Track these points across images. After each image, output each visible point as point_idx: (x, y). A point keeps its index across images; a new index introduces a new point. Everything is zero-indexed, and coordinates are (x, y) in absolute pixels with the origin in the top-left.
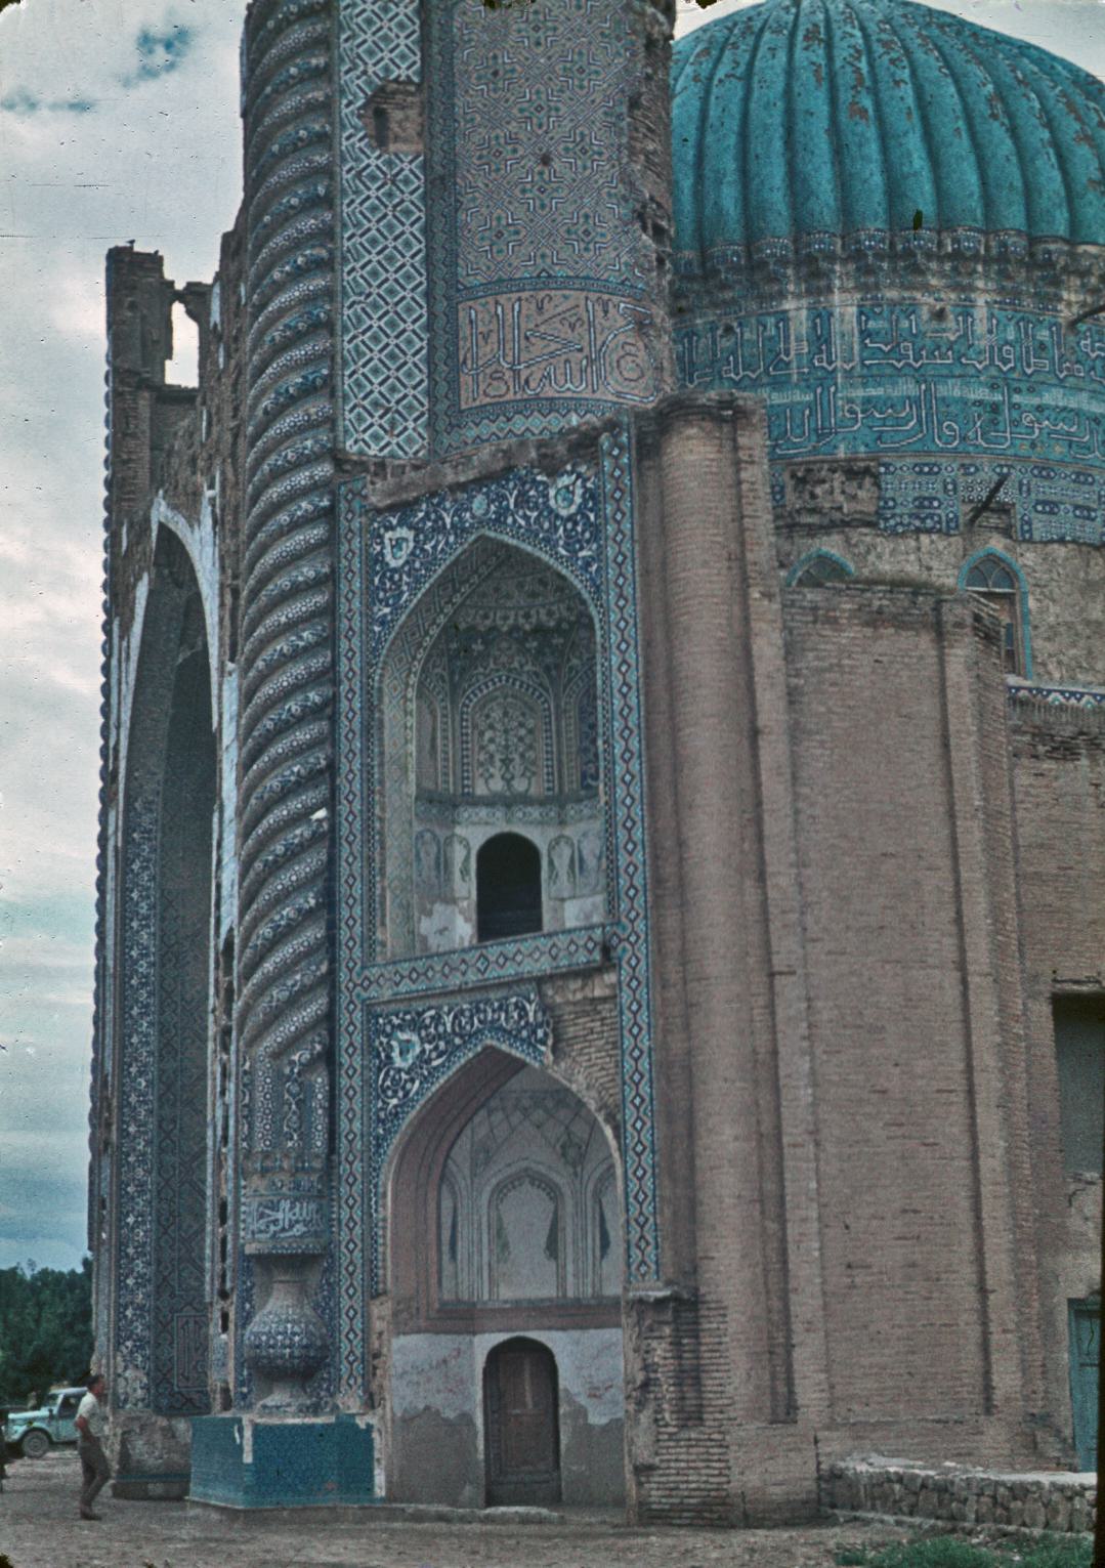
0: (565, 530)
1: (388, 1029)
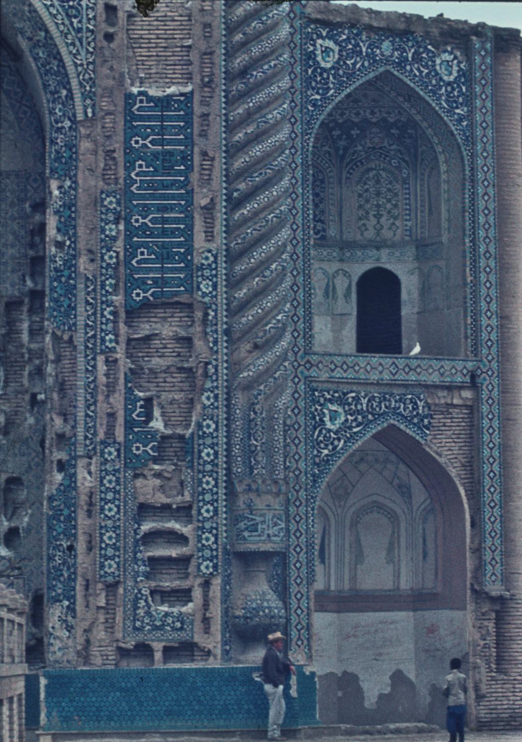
0: (446, 91)
1: (322, 400)
